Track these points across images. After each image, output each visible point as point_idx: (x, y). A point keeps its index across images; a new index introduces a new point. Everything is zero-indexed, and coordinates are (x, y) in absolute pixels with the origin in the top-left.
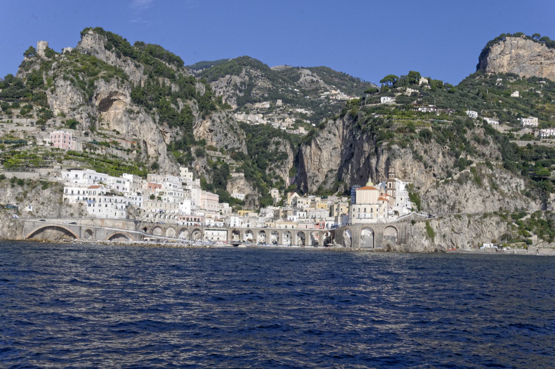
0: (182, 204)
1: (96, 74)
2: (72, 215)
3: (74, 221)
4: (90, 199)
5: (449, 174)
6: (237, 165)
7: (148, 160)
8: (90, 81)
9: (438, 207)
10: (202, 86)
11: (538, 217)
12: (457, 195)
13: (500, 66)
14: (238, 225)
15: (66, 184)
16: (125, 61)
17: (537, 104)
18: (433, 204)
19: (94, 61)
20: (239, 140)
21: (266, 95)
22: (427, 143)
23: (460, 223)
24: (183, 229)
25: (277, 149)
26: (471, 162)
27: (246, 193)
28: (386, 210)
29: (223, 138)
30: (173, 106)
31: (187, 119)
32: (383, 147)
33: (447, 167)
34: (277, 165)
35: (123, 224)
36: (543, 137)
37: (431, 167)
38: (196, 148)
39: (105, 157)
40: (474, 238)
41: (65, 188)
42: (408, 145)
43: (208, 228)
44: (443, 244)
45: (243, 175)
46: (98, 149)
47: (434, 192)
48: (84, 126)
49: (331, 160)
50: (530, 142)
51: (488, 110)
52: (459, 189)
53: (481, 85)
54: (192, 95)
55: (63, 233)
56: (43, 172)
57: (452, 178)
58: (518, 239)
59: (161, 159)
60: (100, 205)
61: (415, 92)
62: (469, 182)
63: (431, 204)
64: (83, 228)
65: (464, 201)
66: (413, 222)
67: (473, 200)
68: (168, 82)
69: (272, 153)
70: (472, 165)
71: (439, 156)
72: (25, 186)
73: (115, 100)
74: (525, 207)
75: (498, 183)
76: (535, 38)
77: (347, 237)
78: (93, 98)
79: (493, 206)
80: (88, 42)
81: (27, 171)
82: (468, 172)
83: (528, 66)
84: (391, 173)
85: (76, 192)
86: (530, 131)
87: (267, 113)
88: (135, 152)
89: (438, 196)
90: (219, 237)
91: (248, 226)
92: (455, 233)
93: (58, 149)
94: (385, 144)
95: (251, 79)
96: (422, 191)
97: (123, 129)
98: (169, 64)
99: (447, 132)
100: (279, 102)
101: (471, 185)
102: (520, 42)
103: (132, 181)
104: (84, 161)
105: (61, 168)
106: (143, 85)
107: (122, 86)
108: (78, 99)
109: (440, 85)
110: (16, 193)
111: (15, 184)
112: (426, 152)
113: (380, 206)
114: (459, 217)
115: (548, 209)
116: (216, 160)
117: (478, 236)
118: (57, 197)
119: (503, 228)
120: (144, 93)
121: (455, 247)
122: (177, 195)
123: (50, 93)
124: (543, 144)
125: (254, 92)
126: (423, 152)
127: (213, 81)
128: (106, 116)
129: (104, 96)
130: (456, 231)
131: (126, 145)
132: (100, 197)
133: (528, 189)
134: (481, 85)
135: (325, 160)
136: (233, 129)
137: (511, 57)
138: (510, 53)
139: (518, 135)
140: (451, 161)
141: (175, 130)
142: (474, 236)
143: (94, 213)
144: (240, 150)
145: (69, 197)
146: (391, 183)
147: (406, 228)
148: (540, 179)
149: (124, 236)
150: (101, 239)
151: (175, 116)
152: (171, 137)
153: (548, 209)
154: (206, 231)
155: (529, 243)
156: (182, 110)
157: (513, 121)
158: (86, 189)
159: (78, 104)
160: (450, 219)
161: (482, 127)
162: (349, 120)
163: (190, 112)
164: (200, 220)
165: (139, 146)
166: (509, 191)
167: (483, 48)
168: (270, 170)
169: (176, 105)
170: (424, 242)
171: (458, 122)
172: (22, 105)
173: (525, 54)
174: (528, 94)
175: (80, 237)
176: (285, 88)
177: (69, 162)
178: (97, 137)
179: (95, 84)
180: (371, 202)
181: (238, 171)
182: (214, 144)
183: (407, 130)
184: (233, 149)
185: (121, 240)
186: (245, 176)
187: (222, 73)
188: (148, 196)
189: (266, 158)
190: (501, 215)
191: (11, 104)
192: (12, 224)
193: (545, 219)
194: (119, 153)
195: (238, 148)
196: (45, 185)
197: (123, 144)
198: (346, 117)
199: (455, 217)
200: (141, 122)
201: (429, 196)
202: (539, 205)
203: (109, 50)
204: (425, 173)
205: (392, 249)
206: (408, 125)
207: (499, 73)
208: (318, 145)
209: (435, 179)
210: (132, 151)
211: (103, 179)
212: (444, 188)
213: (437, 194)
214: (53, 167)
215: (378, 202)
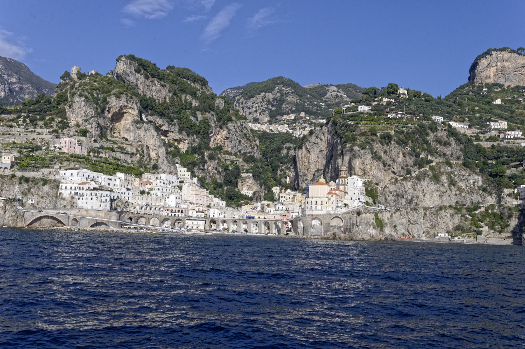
0: (168, 198)
2: (65, 206)
3: (65, 212)
4: (80, 193)
5: (409, 172)
6: (247, 166)
7: (150, 162)
8: (103, 97)
9: (395, 200)
11: (492, 210)
12: (415, 190)
13: (486, 77)
14: (216, 216)
15: (62, 181)
16: (152, 82)
17: (517, 110)
18: (391, 198)
19: (110, 81)
20: (251, 145)
21: (294, 109)
22: (388, 144)
23: (416, 215)
24: (166, 219)
25: (288, 153)
26: (431, 162)
27: (254, 190)
28: (335, 203)
29: (237, 144)
30: (192, 118)
31: (203, 128)
32: (347, 149)
33: (407, 166)
34: (287, 166)
35: (105, 214)
36: (508, 139)
37: (389, 166)
38: (209, 152)
39: (106, 159)
40: (430, 229)
41: (60, 185)
42: (368, 147)
43: (190, 218)
44: (393, 234)
45: (251, 175)
46: (102, 153)
47: (392, 188)
48: (94, 134)
49: (317, 161)
50: (494, 143)
51: (461, 116)
52: (417, 185)
53: (468, 94)
54: (211, 108)
55: (56, 222)
56: (46, 171)
57: (411, 175)
58: (470, 230)
59: (160, 161)
60: (86, 199)
61: (389, 101)
62: (427, 179)
63: (389, 198)
64: (70, 218)
65: (421, 196)
66: (359, 214)
67: (430, 195)
68: (189, 98)
69: (283, 157)
70: (431, 164)
71: (399, 156)
72: (30, 183)
73: (126, 113)
74: (481, 201)
75: (457, 179)
76: (519, 52)
77: (301, 227)
78: (106, 111)
79: (450, 199)
80: (121, 67)
81: (33, 171)
82: (426, 170)
83: (513, 77)
84: (343, 171)
85: (69, 188)
86: (496, 133)
87: (292, 124)
88: (138, 155)
89: (396, 191)
91: (225, 216)
92: (412, 224)
93: (63, 153)
94: (348, 145)
95: (282, 95)
96: (380, 188)
97: (130, 137)
98: (194, 84)
99: (409, 136)
100: (302, 114)
102: (505, 56)
103: (123, 179)
104: (83, 163)
105: (60, 168)
106: (167, 100)
107: (130, 101)
108: (90, 112)
109: (417, 95)
111: (22, 181)
112: (385, 152)
113: (329, 199)
114: (416, 210)
115: (502, 203)
116: (230, 163)
117: (433, 227)
118: (52, 192)
119: (457, 220)
120: (167, 108)
121: (411, 237)
122: (164, 190)
123: (68, 108)
124: (505, 145)
125: (284, 106)
126: (382, 152)
128: (119, 126)
129: (115, 110)
130: (412, 222)
131: (131, 149)
132: (88, 191)
133: (485, 185)
134: (468, 94)
136: (247, 137)
137: (497, 69)
138: (496, 66)
139: (484, 137)
140: (411, 161)
142: (430, 226)
143: (82, 205)
144: (252, 154)
145: (63, 192)
147: (351, 219)
148: (496, 176)
149: (106, 225)
150: (84, 226)
153: (502, 203)
154: (187, 221)
155: (479, 233)
156: (200, 121)
157: (482, 125)
158: (77, 185)
159: (90, 116)
160: (407, 212)
161: (445, 130)
162: (332, 126)
163: (208, 123)
165: (142, 151)
166: (467, 186)
167: (473, 62)
168: (281, 171)
169: (194, 117)
171: (422, 126)
172: (47, 118)
173: (510, 66)
174: (510, 101)
175: (68, 225)
176: (311, 102)
177: (68, 163)
178: (105, 143)
179: (108, 100)
180: (321, 196)
181: (247, 171)
182: (229, 149)
183: (369, 134)
184: (245, 153)
185: (103, 228)
186: (253, 176)
187: (258, 91)
188: (138, 191)
189: (278, 160)
190: (456, 208)
191: (38, 117)
192: (14, 214)
193: (498, 212)
194: (123, 156)
195: (250, 153)
196: (45, 182)
197: (129, 149)
198: (330, 123)
199: (411, 209)
200: (145, 131)
201: (387, 191)
202: (494, 199)
203: (138, 73)
204: (383, 171)
205: (337, 237)
206: (371, 129)
207: (486, 83)
208: (307, 148)
209: (394, 176)
210: (136, 155)
211: (96, 177)
212: (403, 184)
213: (395, 189)
214: (53, 167)
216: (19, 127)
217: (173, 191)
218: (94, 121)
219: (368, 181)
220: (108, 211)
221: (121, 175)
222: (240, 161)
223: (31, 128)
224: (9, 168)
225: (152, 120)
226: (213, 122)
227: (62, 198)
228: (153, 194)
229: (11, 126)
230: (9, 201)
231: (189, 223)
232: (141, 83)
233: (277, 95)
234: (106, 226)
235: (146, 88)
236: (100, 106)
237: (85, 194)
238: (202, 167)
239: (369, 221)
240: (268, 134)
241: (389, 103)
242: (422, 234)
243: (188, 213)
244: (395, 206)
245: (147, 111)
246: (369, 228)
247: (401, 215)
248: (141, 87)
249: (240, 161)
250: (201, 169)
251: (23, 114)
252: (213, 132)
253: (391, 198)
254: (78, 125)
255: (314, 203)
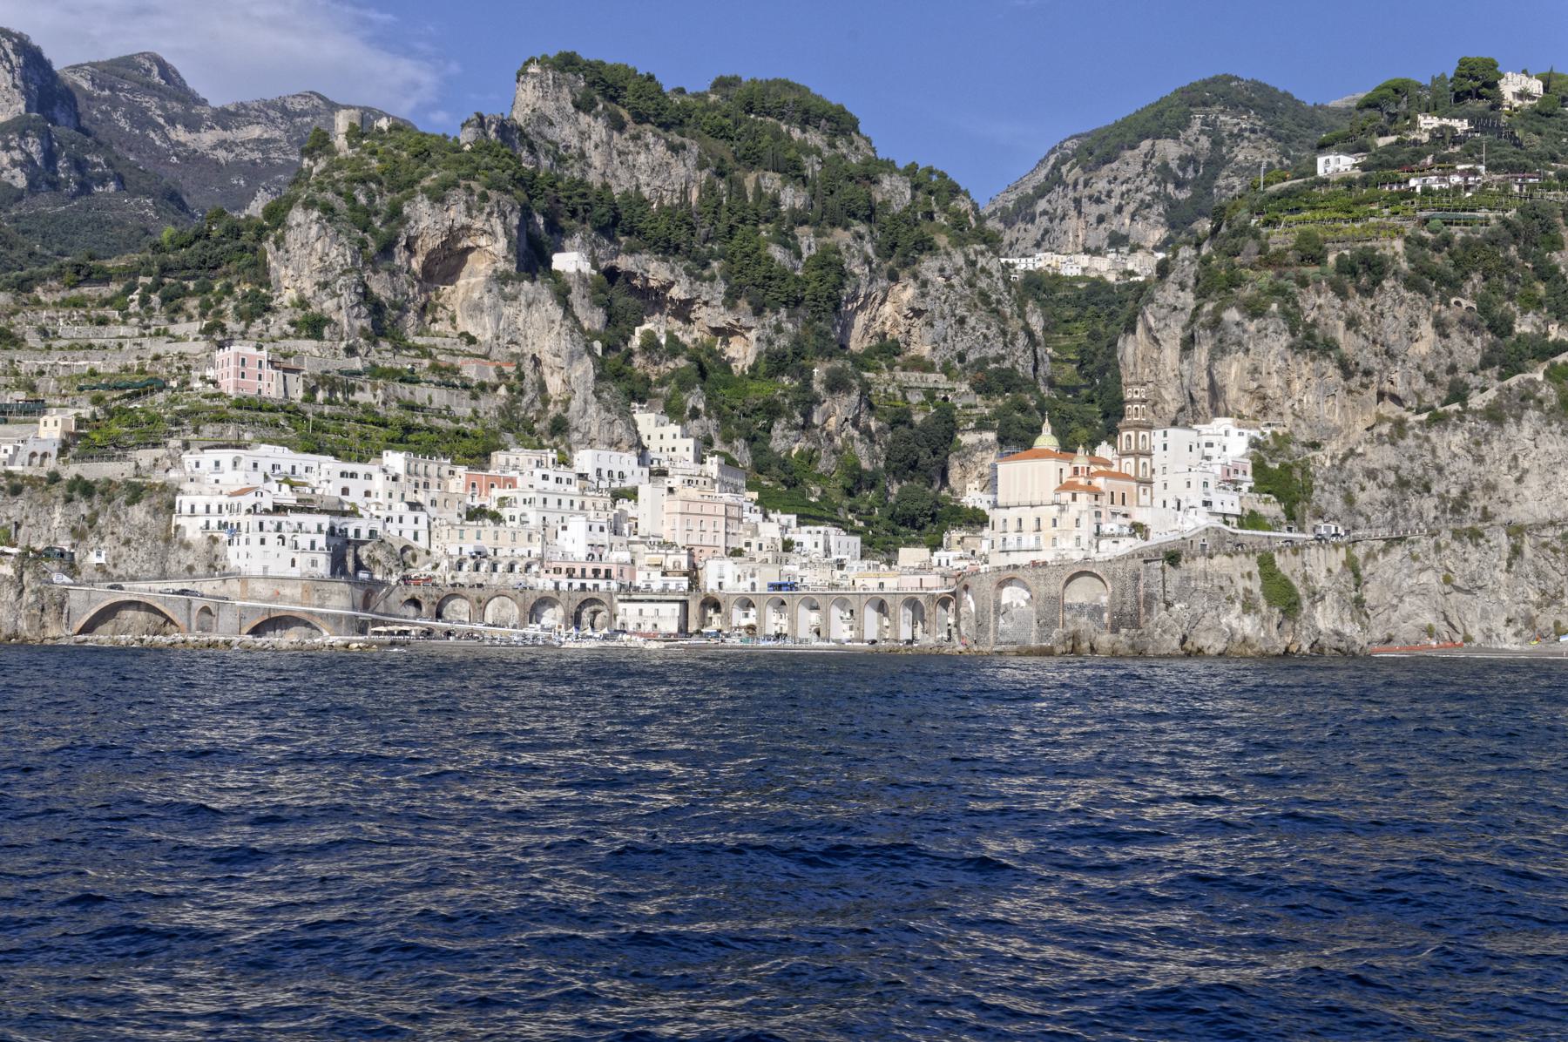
0: (564, 528)
1: (411, 183)
2: (190, 569)
3: (186, 586)
5: (1459, 393)
6: (983, 407)
7: (545, 410)
10: (900, 185)
12: (1480, 460)
15: (187, 487)
18: (1370, 495)
22: (1367, 292)
23: (1474, 555)
24: (545, 602)
29: (950, 332)
30: (777, 253)
33: (1452, 369)
35: (306, 591)
40: (1539, 606)
41: (178, 499)
42: (1274, 307)
44: (1350, 629)
45: (990, 436)
46: (362, 389)
47: (1382, 456)
48: (346, 328)
52: (1487, 441)
55: (161, 620)
56: (145, 457)
59: (575, 405)
60: (247, 542)
61: (1443, 127)
62: (1533, 414)
63: (1362, 498)
65: (1507, 482)
68: (771, 181)
72: (96, 499)
73: (469, 250)
82: (1532, 382)
84: (1131, 401)
85: (200, 508)
88: (502, 391)
89: (1396, 470)
90: (656, 620)
91: (753, 584)
92: (1458, 589)
93: (219, 395)
95: (1217, 143)
96: (1323, 459)
97: (483, 329)
98: (804, 131)
99: (1467, 258)
101: (1538, 425)
106: (694, 195)
108: (340, 255)
110: (74, 517)
112: (1352, 323)
113: (1063, 508)
121: (1459, 639)
122: (552, 503)
125: (1221, 182)
126: (1341, 324)
127: (1105, 163)
129: (432, 242)
130: (1458, 582)
131: (480, 371)
135: (1171, 375)
141: (770, 319)
142: (1534, 597)
144: (1007, 364)
146: (1132, 433)
147: (1137, 578)
149: (307, 624)
151: (770, 278)
152: (758, 339)
154: (621, 606)
158: (224, 500)
159: (338, 271)
164: (614, 573)
165: (520, 378)
169: (786, 246)
170: (1235, 623)
177: (218, 427)
179: (406, 210)
180: (1036, 500)
181: (982, 426)
182: (926, 351)
183: (1291, 257)
184: (983, 361)
185: (287, 639)
187: (1130, 137)
191: (191, 285)
195: (999, 359)
196: (136, 493)
197: (471, 371)
199: (1457, 535)
200: (529, 305)
201: (1356, 469)
203: (587, 111)
204: (1340, 394)
208: (1149, 329)
209: (1388, 409)
210: (495, 388)
211: (300, 470)
212: (1427, 439)
213: (1394, 462)
215: (1058, 498)
216: (124, 323)
217: (588, 505)
218: (347, 286)
219: (1274, 434)
220: (322, 580)
221: (395, 460)
222: (962, 393)
223: (159, 320)
224: (55, 453)
225: (634, 268)
226: (856, 262)
227: (181, 542)
228: (512, 519)
229: (103, 322)
230: (32, 559)
231: (629, 613)
232: (596, 147)
233: (1198, 146)
234: (305, 630)
235: (616, 161)
236: (375, 234)
237: (243, 527)
238: (800, 420)
239: (1225, 583)
240: (1108, 287)
241: (1441, 137)
242: (1502, 629)
243: (633, 576)
244: (1392, 523)
245: (612, 239)
246: (1227, 611)
247: (1415, 559)
248: (596, 159)
249: (962, 393)
250: (796, 427)
251: (142, 279)
252: (862, 293)
253: (1370, 495)
254: (303, 303)
255: (1013, 525)
